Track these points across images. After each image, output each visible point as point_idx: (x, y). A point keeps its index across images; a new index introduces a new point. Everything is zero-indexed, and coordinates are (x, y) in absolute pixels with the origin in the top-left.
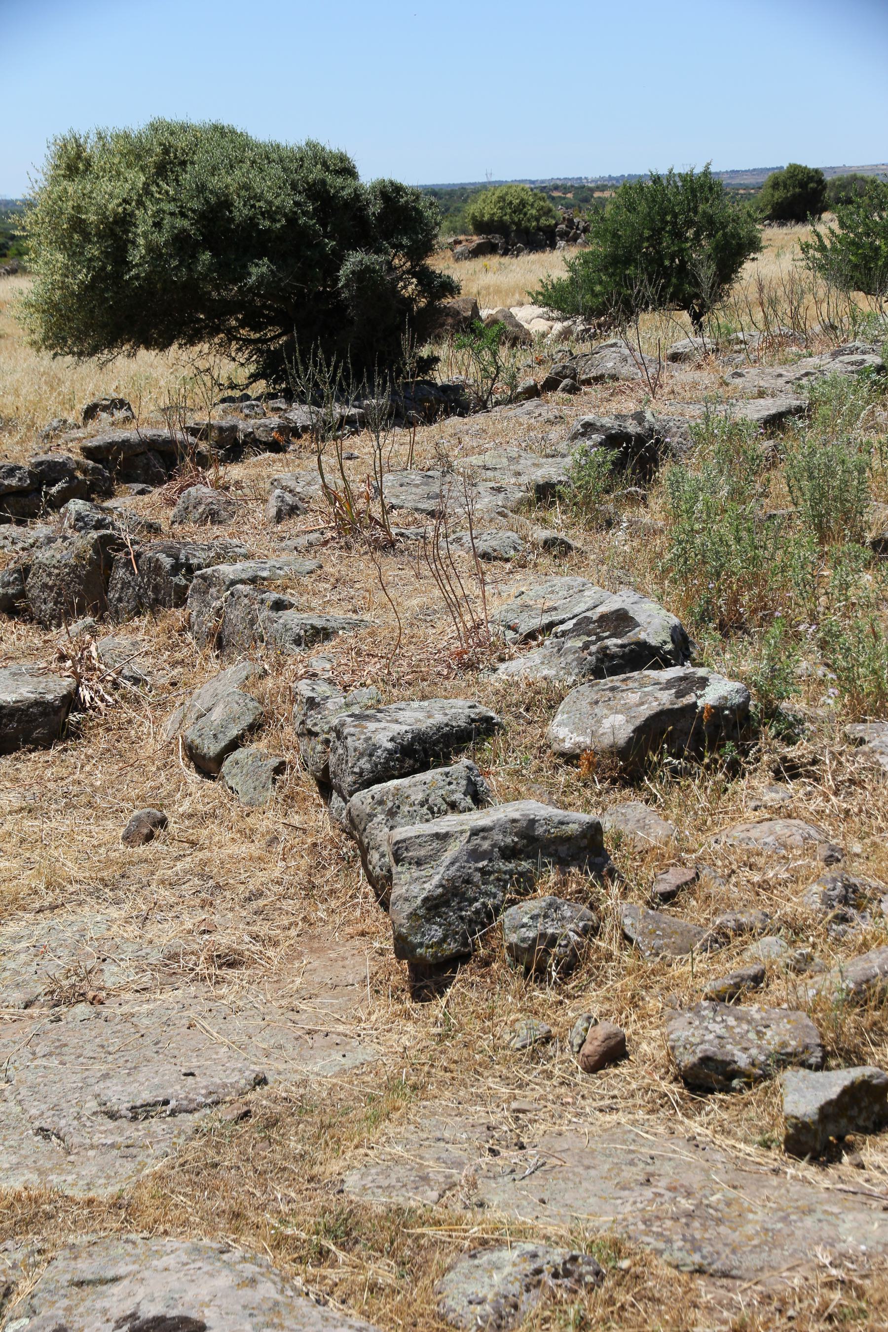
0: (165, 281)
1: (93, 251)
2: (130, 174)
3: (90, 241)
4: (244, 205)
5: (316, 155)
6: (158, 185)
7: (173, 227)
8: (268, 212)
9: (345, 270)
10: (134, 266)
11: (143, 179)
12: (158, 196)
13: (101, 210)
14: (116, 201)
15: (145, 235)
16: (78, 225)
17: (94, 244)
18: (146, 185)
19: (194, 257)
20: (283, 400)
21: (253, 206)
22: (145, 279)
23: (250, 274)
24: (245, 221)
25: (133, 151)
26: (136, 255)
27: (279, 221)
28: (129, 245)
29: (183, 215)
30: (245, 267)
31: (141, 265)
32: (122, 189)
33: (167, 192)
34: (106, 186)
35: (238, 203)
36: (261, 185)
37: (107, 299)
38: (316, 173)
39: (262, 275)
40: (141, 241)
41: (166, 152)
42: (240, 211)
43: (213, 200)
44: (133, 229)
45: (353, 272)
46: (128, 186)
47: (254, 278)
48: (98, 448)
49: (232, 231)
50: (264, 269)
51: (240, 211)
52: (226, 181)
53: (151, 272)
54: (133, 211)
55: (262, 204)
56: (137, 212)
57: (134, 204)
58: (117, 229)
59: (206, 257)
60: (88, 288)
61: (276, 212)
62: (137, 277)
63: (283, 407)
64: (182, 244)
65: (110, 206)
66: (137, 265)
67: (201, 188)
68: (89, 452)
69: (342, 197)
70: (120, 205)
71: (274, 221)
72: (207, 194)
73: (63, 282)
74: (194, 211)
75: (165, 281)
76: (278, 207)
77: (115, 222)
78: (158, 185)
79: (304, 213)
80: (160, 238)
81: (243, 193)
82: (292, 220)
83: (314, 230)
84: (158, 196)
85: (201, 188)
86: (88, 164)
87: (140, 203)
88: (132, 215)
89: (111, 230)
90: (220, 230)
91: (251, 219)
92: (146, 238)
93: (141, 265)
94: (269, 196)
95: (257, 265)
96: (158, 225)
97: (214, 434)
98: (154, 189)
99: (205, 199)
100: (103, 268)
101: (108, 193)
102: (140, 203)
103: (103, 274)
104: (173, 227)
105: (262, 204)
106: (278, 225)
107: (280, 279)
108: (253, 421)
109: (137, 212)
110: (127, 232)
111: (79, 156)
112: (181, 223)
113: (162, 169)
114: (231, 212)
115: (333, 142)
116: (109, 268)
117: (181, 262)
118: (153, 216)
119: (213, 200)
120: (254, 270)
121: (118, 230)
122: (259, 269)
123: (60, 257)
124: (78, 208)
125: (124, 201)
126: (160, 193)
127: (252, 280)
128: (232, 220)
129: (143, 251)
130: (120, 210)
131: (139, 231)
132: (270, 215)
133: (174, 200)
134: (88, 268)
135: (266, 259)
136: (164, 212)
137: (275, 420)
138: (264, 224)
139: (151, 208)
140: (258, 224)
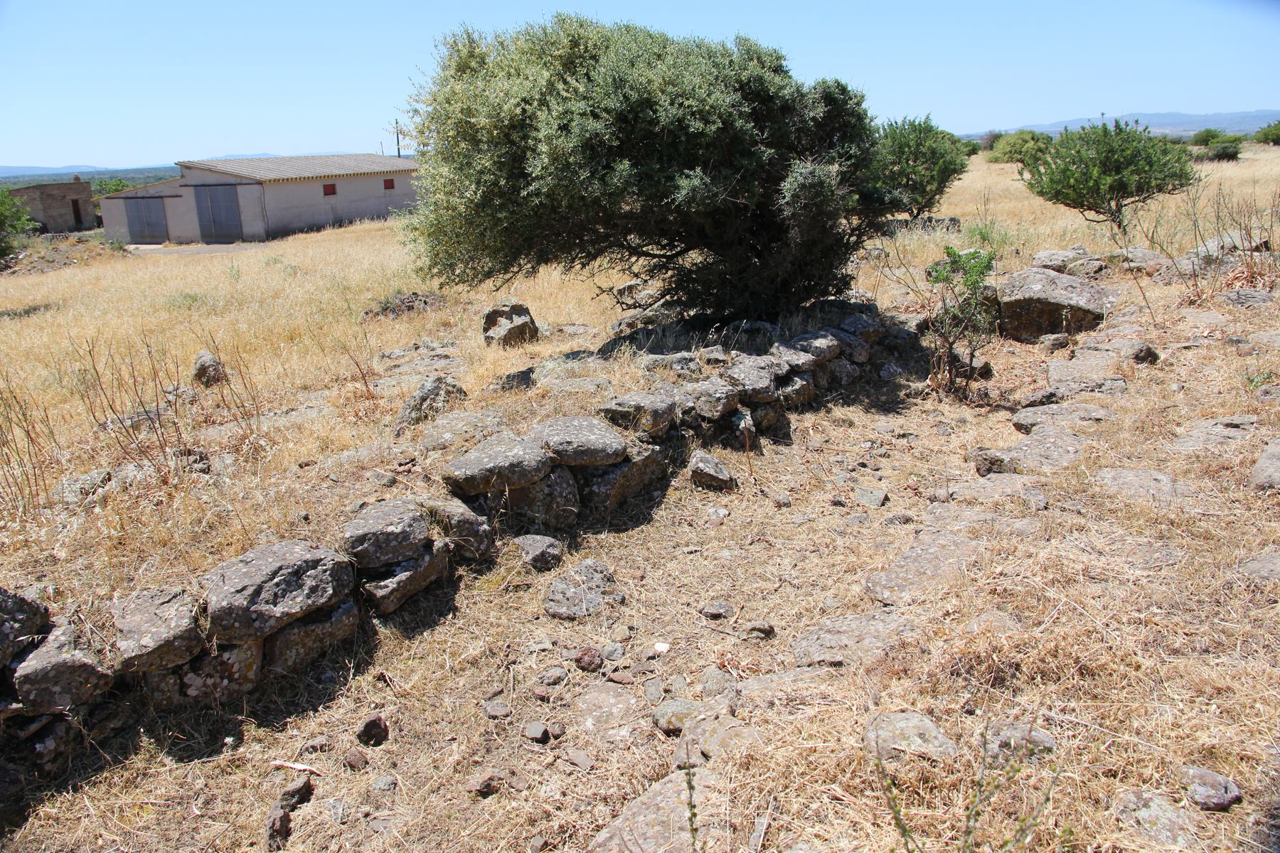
0: (572, 197)
1: (485, 161)
2: (531, 71)
3: (479, 151)
4: (672, 104)
5: (751, 53)
6: (565, 82)
7: (584, 130)
8: (700, 112)
9: (788, 186)
10: (534, 180)
11: (546, 74)
12: (565, 94)
13: (496, 114)
14: (513, 101)
15: (549, 139)
16: (468, 132)
17: (485, 152)
18: (551, 84)
19: (609, 167)
20: (719, 347)
21: (681, 105)
22: (548, 196)
23: (678, 188)
24: (672, 123)
25: (539, 47)
26: (535, 167)
27: (714, 123)
28: (529, 153)
29: (596, 116)
30: (672, 178)
31: (542, 178)
32: (519, 88)
33: (576, 91)
34: (501, 84)
35: (664, 100)
36: (691, 80)
37: (499, 219)
38: (753, 68)
39: (694, 189)
40: (543, 148)
41: (575, 43)
42: (666, 113)
43: (634, 96)
44: (534, 134)
45: (803, 186)
46: (528, 84)
47: (684, 192)
48: (470, 480)
49: (657, 134)
50: (696, 182)
51: (666, 113)
52: (651, 76)
53: (555, 186)
54: (534, 114)
55: (691, 102)
56: (539, 113)
57: (536, 103)
58: (514, 135)
59: (624, 166)
60: (484, 204)
61: (708, 112)
62: (537, 193)
63: (721, 357)
64: (592, 149)
65: (505, 107)
66: (537, 178)
67: (619, 83)
68: (459, 488)
69: (783, 97)
70: (518, 105)
71: (707, 122)
72: (627, 90)
73: (448, 202)
74: (606, 110)
75: (572, 197)
76: (712, 107)
77: (512, 126)
78: (565, 82)
79: (741, 114)
80: (568, 144)
81: (670, 89)
82: (728, 123)
83: (752, 135)
84: (565, 94)
85: (619, 83)
86: (483, 62)
87: (543, 103)
88: (533, 117)
89: (507, 135)
90: (642, 135)
91: (679, 120)
92: (549, 143)
93: (542, 178)
94: (702, 93)
95: (688, 176)
96: (564, 128)
97: (646, 421)
98: (560, 86)
99: (624, 96)
100: (496, 184)
101: (502, 95)
102: (543, 103)
103: (496, 190)
104: (584, 130)
105: (691, 102)
106: (714, 128)
107: (716, 195)
108: (689, 387)
109: (539, 113)
110: (525, 137)
111: (471, 55)
112: (597, 126)
113: (569, 64)
114: (655, 112)
115: (766, 41)
116: (503, 182)
117: (593, 174)
118: (559, 117)
119: (634, 96)
120: (683, 182)
121: (515, 136)
122: (690, 183)
123: (445, 170)
124: (468, 112)
125: (524, 100)
126: (567, 91)
127: (681, 196)
128: (655, 122)
129: (546, 160)
130: (518, 111)
131: (541, 135)
132: (705, 117)
133: (585, 98)
134: (478, 183)
135: (698, 169)
136: (572, 113)
137: (717, 386)
138: (696, 125)
139: (557, 109)
140: (688, 126)
